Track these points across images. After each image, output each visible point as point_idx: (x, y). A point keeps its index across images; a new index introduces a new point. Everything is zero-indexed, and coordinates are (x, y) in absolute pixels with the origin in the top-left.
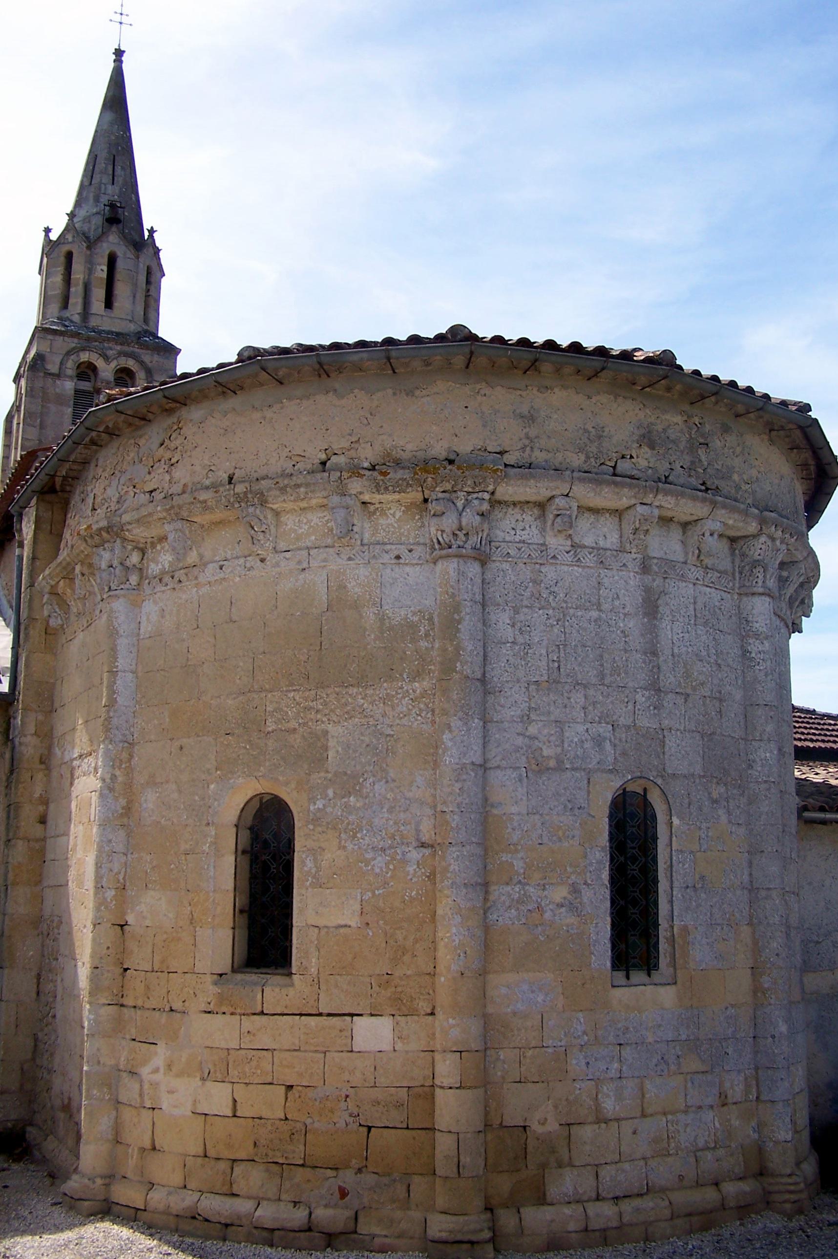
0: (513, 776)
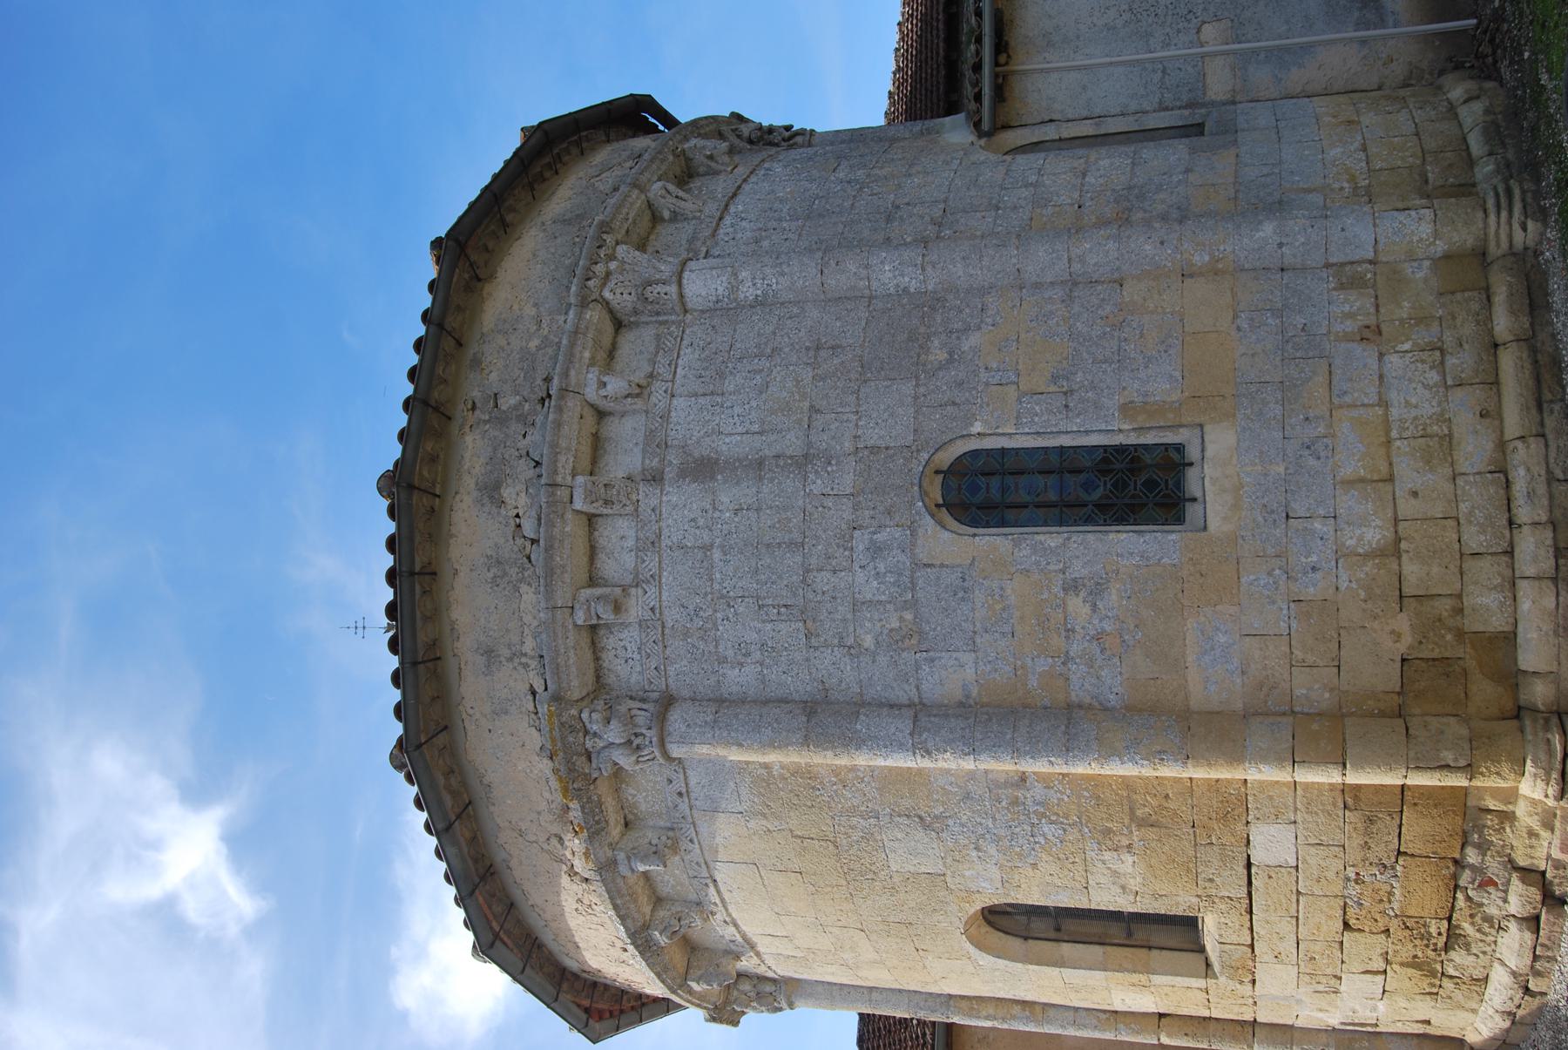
0: (928, 670)
